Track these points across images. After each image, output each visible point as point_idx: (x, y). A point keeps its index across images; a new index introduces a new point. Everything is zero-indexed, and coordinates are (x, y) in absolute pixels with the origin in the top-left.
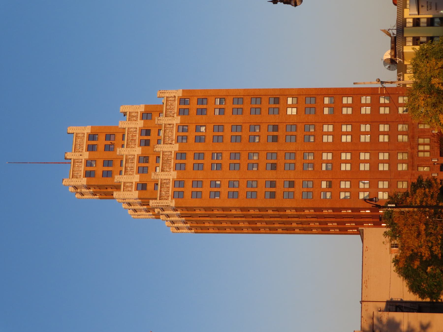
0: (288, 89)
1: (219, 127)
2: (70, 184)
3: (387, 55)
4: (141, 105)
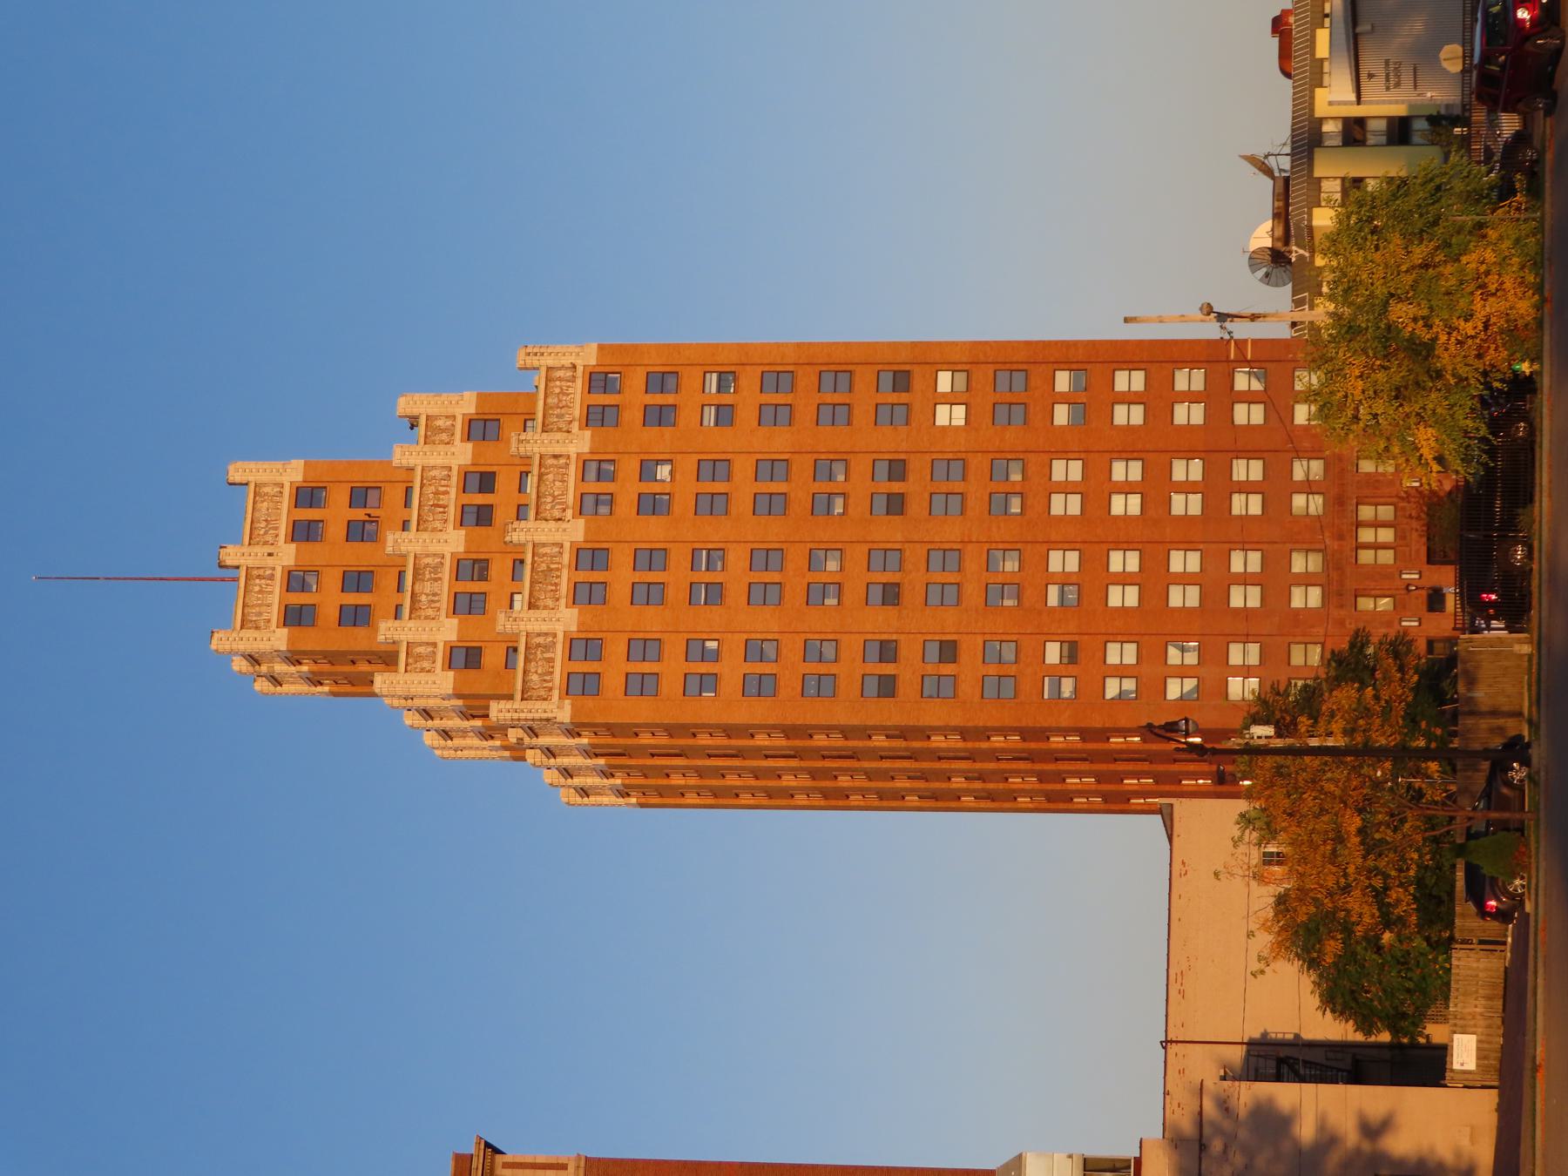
1: (716, 467)
2: (234, 646)
3: (1262, 236)
4: (467, 394)
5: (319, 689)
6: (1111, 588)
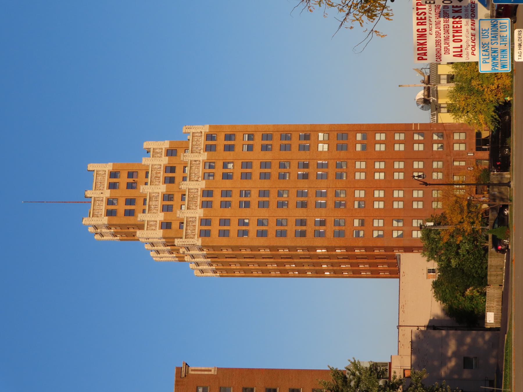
0: (319, 125)
1: (247, 165)
2: (90, 223)
3: (421, 95)
4: (166, 141)
5: (116, 238)
6: (375, 202)
